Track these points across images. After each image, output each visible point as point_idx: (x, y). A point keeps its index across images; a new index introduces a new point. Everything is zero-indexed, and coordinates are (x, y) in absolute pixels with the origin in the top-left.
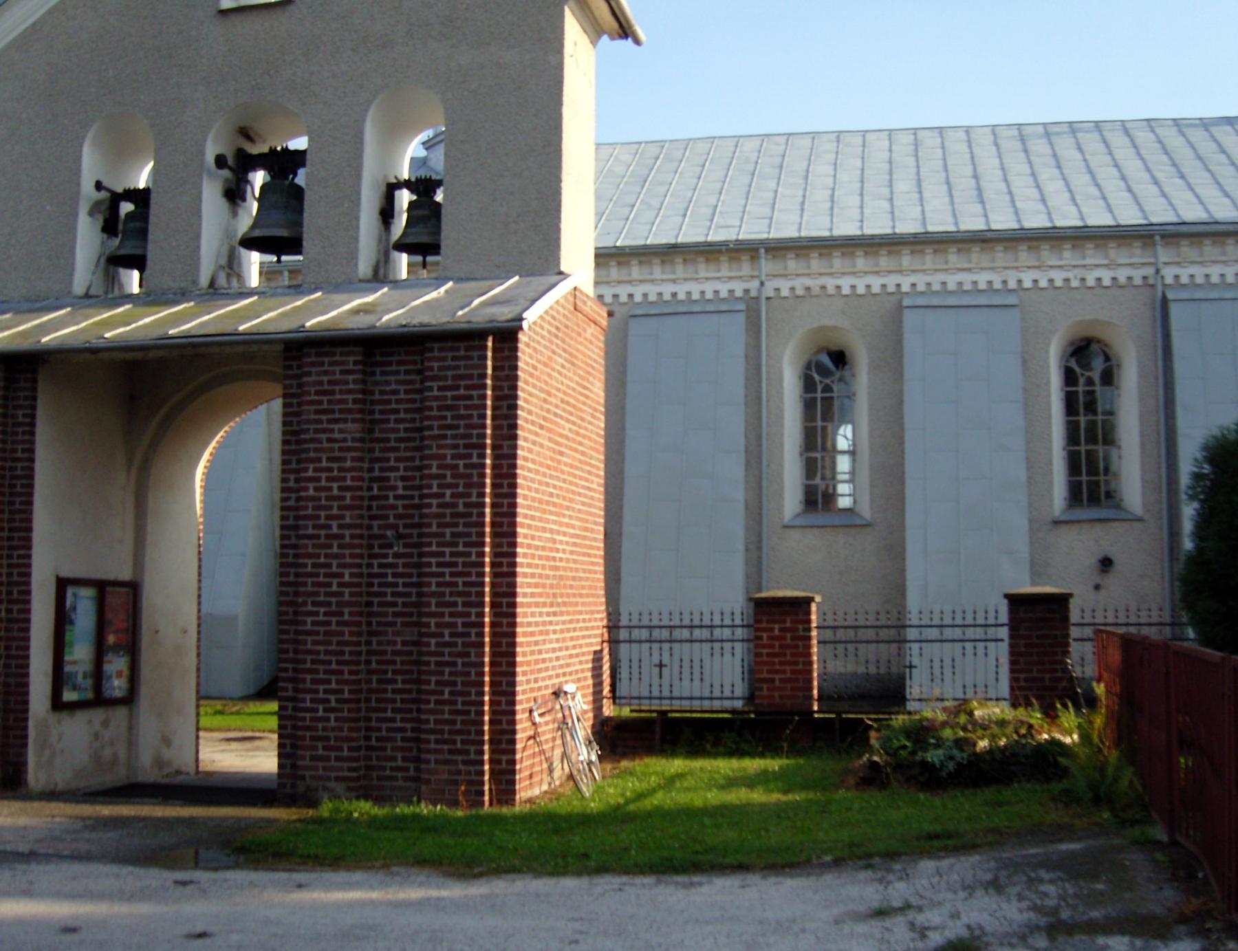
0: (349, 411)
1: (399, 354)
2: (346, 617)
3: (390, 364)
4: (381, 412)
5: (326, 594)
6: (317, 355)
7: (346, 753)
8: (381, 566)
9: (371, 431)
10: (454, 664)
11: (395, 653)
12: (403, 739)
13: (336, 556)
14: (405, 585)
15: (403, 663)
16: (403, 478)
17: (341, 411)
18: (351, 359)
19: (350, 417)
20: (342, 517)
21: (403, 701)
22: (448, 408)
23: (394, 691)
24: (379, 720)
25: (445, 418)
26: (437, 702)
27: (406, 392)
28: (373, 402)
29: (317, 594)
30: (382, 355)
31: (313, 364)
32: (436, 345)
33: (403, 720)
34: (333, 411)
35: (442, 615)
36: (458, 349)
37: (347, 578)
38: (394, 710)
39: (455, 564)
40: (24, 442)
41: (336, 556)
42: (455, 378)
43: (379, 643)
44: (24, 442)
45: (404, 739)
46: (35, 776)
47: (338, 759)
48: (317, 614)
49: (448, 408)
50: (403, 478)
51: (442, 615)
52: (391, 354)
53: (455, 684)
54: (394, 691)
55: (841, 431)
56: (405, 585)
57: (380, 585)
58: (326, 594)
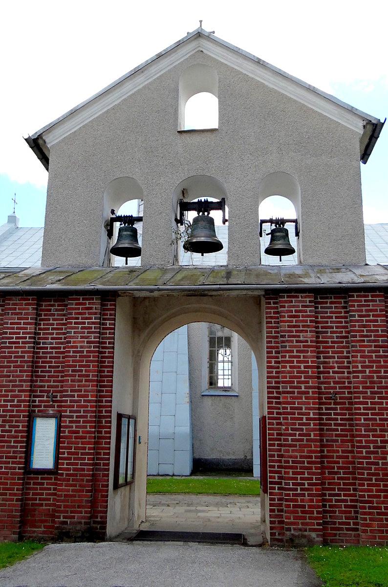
0: (308, 326)
1: (331, 298)
2: (312, 437)
3: (326, 303)
4: (322, 327)
5: (300, 424)
6: (288, 297)
7: (315, 515)
8: (327, 409)
9: (318, 337)
10: (378, 464)
11: (338, 457)
12: (346, 506)
13: (304, 403)
14: (341, 419)
15: (343, 463)
16: (337, 362)
17: (303, 326)
18: (308, 299)
19: (308, 329)
20: (308, 382)
21: (344, 484)
22: (364, 326)
23: (339, 478)
24: (330, 495)
25: (363, 331)
26: (368, 485)
27: (336, 317)
28: (39, 338)
29: (295, 424)
30: (321, 298)
31: (286, 302)
32: (355, 294)
33: (345, 495)
34: (299, 326)
35: (368, 436)
36: (368, 296)
37: (312, 416)
38: (339, 489)
39: (374, 409)
40: (109, 338)
41: (304, 403)
42: (367, 311)
43: (328, 451)
44: (109, 338)
45: (346, 506)
46: (110, 530)
47: (310, 518)
48: (11, 406)
49: (364, 326)
50: (337, 362)
51: (368, 436)
52: (327, 298)
53: (378, 474)
54: (339, 478)
55: (220, 352)
56: (341, 419)
57: (327, 419)
58: (300, 424)
